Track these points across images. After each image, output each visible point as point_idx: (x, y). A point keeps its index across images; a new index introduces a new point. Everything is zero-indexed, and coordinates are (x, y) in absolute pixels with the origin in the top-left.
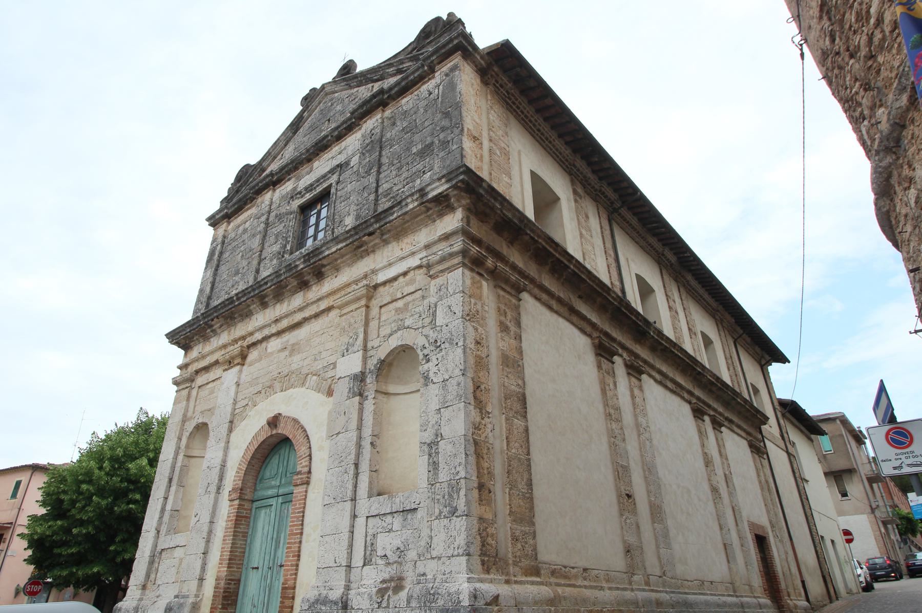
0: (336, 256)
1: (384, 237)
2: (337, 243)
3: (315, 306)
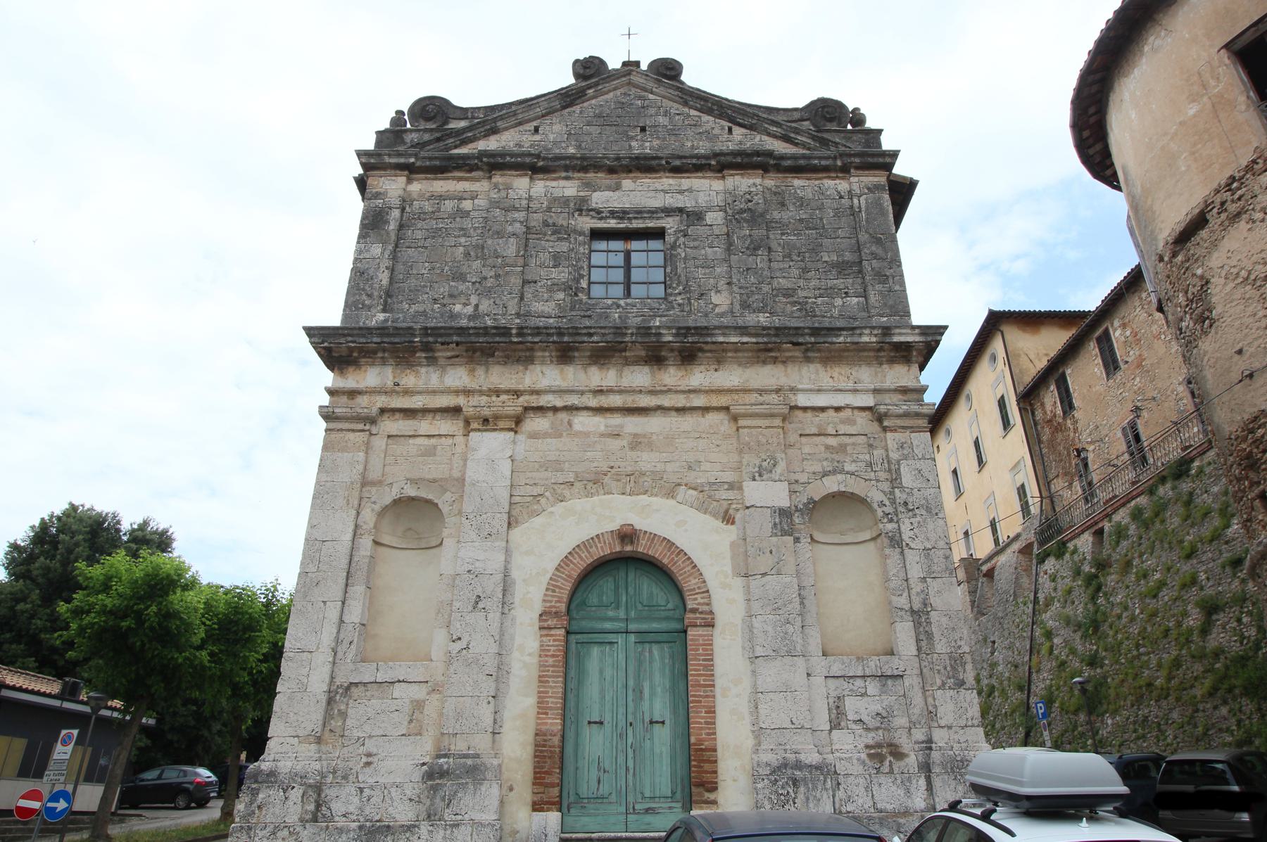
0: (730, 346)
1: (810, 354)
2: (742, 335)
3: (682, 396)
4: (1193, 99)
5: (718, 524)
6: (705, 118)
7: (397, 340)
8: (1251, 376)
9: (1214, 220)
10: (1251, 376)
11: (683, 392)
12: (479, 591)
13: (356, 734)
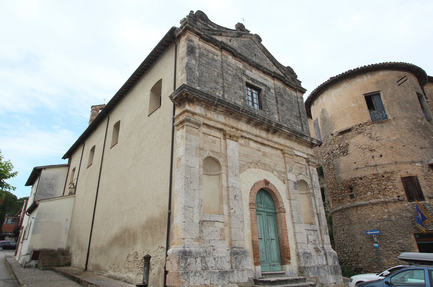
2: (288, 130)
4: (354, 102)
5: (282, 183)
6: (268, 59)
7: (210, 100)
8: (357, 169)
9: (353, 132)
10: (357, 169)
11: (274, 142)
12: (235, 193)
13: (207, 239)
